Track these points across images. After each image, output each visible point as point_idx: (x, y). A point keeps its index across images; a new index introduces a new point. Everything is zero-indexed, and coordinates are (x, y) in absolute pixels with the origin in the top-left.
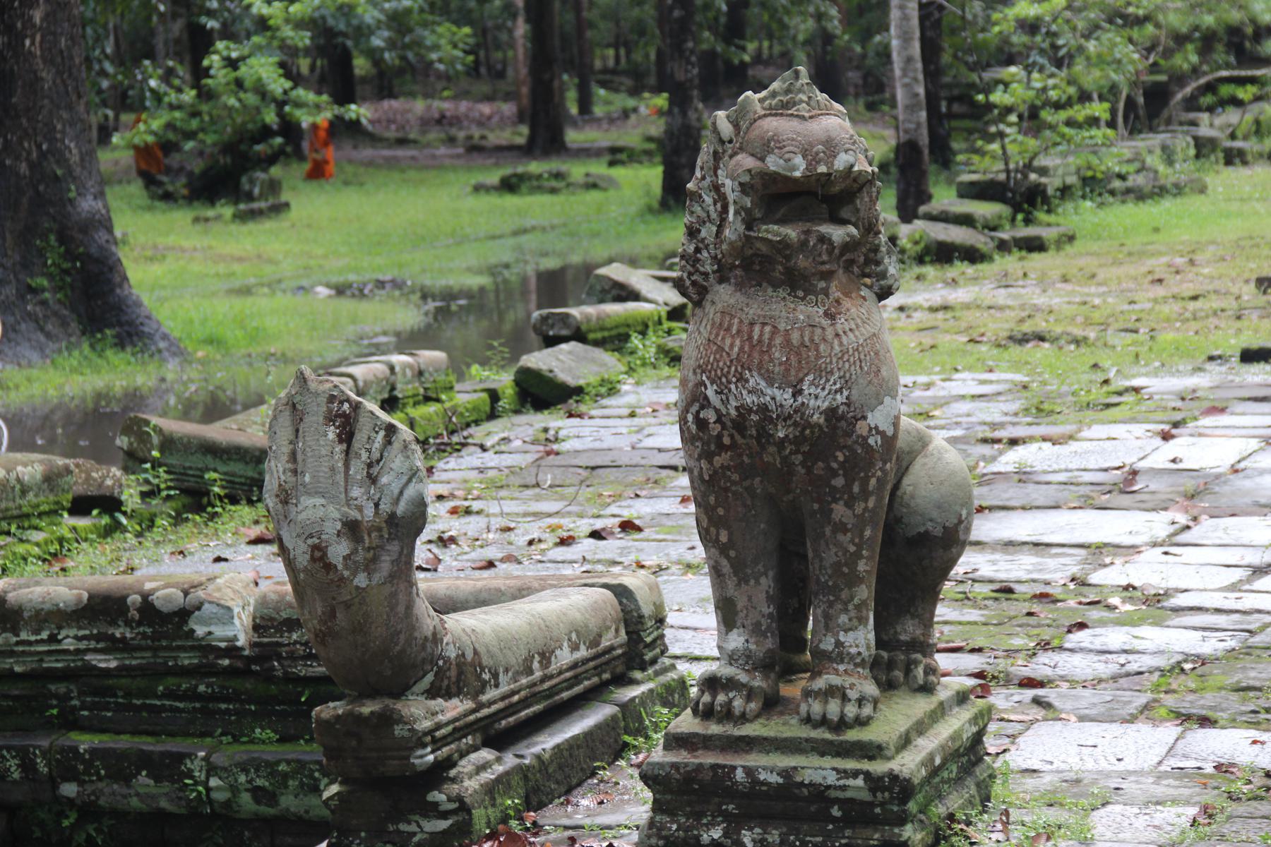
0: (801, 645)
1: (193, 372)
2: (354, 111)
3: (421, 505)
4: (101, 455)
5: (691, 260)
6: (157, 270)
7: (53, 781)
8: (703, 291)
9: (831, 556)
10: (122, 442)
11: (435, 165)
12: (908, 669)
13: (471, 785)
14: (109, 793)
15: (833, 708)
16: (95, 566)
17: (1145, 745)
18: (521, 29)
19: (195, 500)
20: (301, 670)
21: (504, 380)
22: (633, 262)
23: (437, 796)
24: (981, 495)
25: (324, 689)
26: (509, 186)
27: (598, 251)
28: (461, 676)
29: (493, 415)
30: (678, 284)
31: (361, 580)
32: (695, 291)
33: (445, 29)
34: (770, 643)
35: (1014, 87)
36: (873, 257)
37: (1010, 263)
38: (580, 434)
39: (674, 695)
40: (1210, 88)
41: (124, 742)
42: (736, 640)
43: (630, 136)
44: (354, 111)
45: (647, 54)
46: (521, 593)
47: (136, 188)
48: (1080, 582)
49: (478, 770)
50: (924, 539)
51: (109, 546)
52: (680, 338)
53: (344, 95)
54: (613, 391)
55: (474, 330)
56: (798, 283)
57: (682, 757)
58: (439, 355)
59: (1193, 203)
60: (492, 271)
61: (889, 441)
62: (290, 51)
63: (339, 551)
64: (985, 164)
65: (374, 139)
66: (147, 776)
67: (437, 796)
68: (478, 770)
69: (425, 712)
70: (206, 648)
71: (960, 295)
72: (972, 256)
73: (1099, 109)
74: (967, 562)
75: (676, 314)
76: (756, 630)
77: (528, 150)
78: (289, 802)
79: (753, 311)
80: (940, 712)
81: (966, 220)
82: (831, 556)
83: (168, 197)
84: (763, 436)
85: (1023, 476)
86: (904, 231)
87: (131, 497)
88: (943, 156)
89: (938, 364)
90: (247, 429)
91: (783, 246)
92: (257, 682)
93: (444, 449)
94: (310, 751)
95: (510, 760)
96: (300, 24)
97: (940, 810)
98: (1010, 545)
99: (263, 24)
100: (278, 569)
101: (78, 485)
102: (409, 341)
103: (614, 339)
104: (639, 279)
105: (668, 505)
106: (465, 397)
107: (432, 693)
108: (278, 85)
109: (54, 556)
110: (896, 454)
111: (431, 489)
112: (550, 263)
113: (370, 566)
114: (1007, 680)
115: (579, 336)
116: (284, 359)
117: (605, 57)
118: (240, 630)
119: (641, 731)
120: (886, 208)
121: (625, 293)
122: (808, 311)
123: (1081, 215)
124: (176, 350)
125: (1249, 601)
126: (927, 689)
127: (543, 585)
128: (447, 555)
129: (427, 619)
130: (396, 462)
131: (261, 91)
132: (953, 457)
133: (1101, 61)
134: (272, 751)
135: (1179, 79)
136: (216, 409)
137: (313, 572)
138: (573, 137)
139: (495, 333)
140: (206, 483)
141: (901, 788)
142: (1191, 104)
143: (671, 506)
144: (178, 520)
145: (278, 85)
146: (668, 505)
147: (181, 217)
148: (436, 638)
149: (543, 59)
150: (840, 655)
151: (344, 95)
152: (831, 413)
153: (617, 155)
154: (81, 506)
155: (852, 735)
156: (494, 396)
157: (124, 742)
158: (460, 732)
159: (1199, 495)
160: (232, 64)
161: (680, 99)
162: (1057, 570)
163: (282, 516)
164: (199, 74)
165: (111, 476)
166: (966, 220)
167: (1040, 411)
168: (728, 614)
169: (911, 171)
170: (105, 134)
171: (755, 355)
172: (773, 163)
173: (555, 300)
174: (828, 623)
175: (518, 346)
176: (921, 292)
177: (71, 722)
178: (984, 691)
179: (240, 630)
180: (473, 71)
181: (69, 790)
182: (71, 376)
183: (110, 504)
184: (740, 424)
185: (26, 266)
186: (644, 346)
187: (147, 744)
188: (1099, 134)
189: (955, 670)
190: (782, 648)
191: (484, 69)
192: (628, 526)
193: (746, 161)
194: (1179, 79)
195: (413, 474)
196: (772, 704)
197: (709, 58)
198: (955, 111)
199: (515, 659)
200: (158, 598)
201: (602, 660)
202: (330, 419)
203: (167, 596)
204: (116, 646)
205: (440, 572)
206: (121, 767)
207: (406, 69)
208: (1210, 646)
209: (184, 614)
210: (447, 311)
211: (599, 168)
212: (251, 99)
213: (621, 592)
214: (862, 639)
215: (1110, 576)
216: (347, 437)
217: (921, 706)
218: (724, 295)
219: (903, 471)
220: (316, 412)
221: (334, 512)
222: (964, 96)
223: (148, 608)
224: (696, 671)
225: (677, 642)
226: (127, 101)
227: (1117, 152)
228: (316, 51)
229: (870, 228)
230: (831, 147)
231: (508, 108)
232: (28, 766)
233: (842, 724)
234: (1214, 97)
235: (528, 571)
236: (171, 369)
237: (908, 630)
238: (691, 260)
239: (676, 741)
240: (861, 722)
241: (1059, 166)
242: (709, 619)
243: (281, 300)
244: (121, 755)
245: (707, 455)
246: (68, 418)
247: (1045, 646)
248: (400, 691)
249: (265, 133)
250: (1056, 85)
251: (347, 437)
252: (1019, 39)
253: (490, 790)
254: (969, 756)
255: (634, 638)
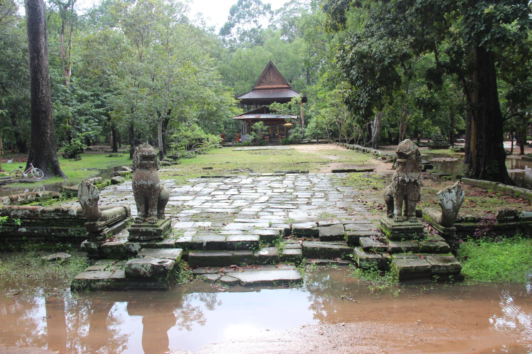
0: (148, 214)
1: (69, 180)
2: (91, 147)
3: (99, 197)
4: (56, 190)
5: (133, 165)
6: (64, 167)
7: (51, 233)
8: (135, 169)
9: (152, 202)
10: (59, 189)
11: (101, 154)
12: (161, 216)
13: (106, 232)
14: (58, 234)
15: (152, 221)
16: (56, 205)
17: (190, 224)
18: (112, 137)
19: (69, 197)
20: (83, 218)
21: (110, 181)
22: (126, 166)
23: (101, 234)
24: (170, 194)
25: (86, 221)
26: (110, 156)
27: (122, 165)
28: (104, 218)
29: (108, 185)
30: (132, 169)
31: (91, 207)
32: (134, 169)
33: (102, 137)
34: (144, 213)
35: (173, 145)
36: (156, 165)
37: (173, 166)
38: (119, 187)
39: (132, 220)
40: (197, 145)
41: (60, 228)
42: (140, 213)
43: (126, 150)
44: (91, 147)
45: (128, 140)
46: (112, 208)
47: (62, 157)
48: (182, 205)
49: (107, 230)
50: (163, 200)
51: (58, 203)
52: (132, 175)
53: (89, 145)
54: (124, 182)
55: (106, 174)
56: (147, 168)
57: (133, 228)
58: (101, 178)
59: (195, 159)
60: (108, 167)
61: (159, 188)
62: (82, 140)
63: (88, 203)
64: (170, 154)
65: (92, 150)
66: (528, 167)
67: (101, 234)
68: (107, 230)
69: (99, 223)
70: (71, 216)
71: (167, 170)
72: (169, 165)
73: (184, 147)
74: (169, 203)
75: (132, 172)
76: (142, 212)
77: (113, 152)
78: (82, 235)
79: (142, 172)
80: (165, 221)
81: (168, 161)
82: (152, 202)
83: (66, 158)
84: (143, 187)
85: (175, 192)
86: (160, 162)
87: (60, 196)
88: (165, 153)
89: (165, 178)
90: (76, 187)
91: (145, 164)
92: (78, 220)
93: (102, 190)
94: (85, 228)
95: (111, 229)
96: (83, 136)
97: (165, 233)
98: (174, 201)
99: (78, 136)
100: (80, 205)
101: (53, 195)
102: (97, 176)
103: (124, 175)
104: (127, 168)
105: (131, 196)
106: (104, 183)
107: (100, 221)
108: (80, 144)
109: (50, 204)
110: (160, 190)
111: (100, 195)
112: (116, 166)
113: (92, 205)
114: (174, 217)
115: (119, 175)
116: (81, 178)
117: (123, 140)
118: (75, 213)
119: (128, 225)
120: (158, 159)
121: (125, 170)
122: (148, 172)
123: (182, 160)
124: (67, 178)
125: (202, 207)
126: (164, 219)
127: (115, 207)
128: (102, 203)
129: (100, 211)
130: (95, 191)
131: (78, 145)
132: (167, 190)
133: (184, 142)
134: (79, 228)
135: (193, 144)
136: (72, 185)
137: (84, 206)
138: (118, 150)
139: (108, 175)
140: (70, 194)
141: (161, 231)
142: (194, 147)
143: (131, 196)
144: (67, 199)
145: (80, 144)
146: (131, 196)
147: (67, 160)
148: (101, 214)
149: (115, 140)
150: (153, 215)
151: (89, 145)
152: (151, 185)
153: (124, 152)
154: (54, 197)
155: (155, 225)
156: (108, 183)
157: (60, 228)
158: (104, 226)
159: (196, 194)
160: (74, 141)
161: (132, 146)
162: (180, 203)
163: (80, 199)
164: (70, 142)
165: (58, 194)
166: (168, 161)
167: (177, 184)
168: (139, 210)
169: (161, 155)
170: (57, 150)
171: (142, 178)
172: (144, 153)
173: (116, 170)
174: (151, 211)
175: (111, 176)
176: (162, 169)
177: (53, 225)
178: (171, 218)
179: (75, 213)
180: (106, 142)
181: (53, 234)
182: (53, 181)
183: (58, 197)
184: (140, 186)
185: (47, 167)
186: (128, 176)
187: (63, 228)
188: (184, 150)
189: (167, 216)
190: (145, 212)
191: (107, 142)
192: (126, 199)
193: (140, 153)
194: (193, 144)
195: (97, 193)
196: (144, 221)
197: (136, 141)
198: (166, 147)
199: (111, 216)
200: (64, 209)
201: (122, 216)
202: (86, 186)
203: (65, 209)
204: (58, 215)
205: (101, 205)
206: (60, 231)
207: (97, 142)
208: (198, 212)
209: (68, 211)
210: (102, 172)
211: (122, 154)
212: (77, 145)
213: (125, 207)
214: (156, 213)
215: (186, 204)
216: (89, 188)
217: (163, 221)
218: (138, 170)
219: (161, 192)
220: (85, 185)
221: (87, 198)
222: (167, 146)
223: (63, 211)
224: (135, 217)
225: (132, 214)
226: (60, 146)
227: (186, 153)
228: (85, 139)
229: (156, 162)
230: (151, 152)
231: (110, 147)
232: (47, 231)
233: (153, 223)
234: (197, 146)
235: (113, 205)
236: (66, 180)
237: (161, 211)
238: (133, 165)
239: (132, 226)
240: (156, 223)
241: (179, 154)
242: (136, 211)
243: (80, 171)
244: (60, 229)
245: (136, 190)
246: (53, 186)
247: (178, 213)
248: (96, 220)
249: (78, 150)
250: (179, 145)
251: (89, 188)
252: (174, 139)
253: (108, 233)
254: (169, 226)
255: (127, 213)
